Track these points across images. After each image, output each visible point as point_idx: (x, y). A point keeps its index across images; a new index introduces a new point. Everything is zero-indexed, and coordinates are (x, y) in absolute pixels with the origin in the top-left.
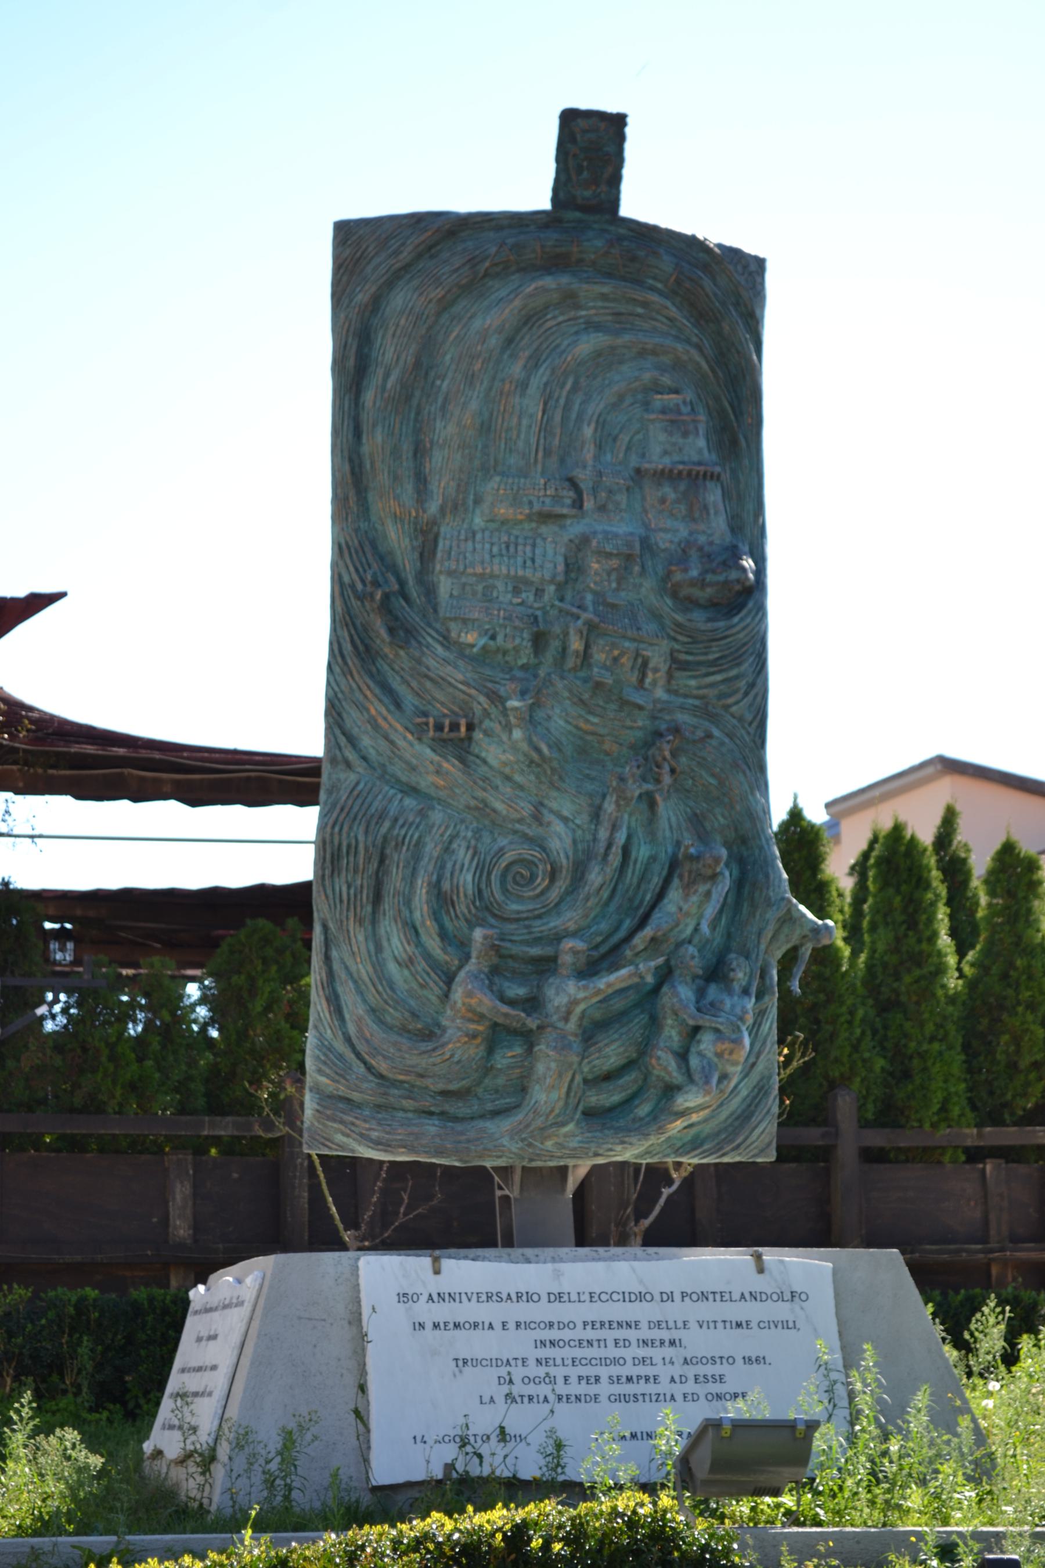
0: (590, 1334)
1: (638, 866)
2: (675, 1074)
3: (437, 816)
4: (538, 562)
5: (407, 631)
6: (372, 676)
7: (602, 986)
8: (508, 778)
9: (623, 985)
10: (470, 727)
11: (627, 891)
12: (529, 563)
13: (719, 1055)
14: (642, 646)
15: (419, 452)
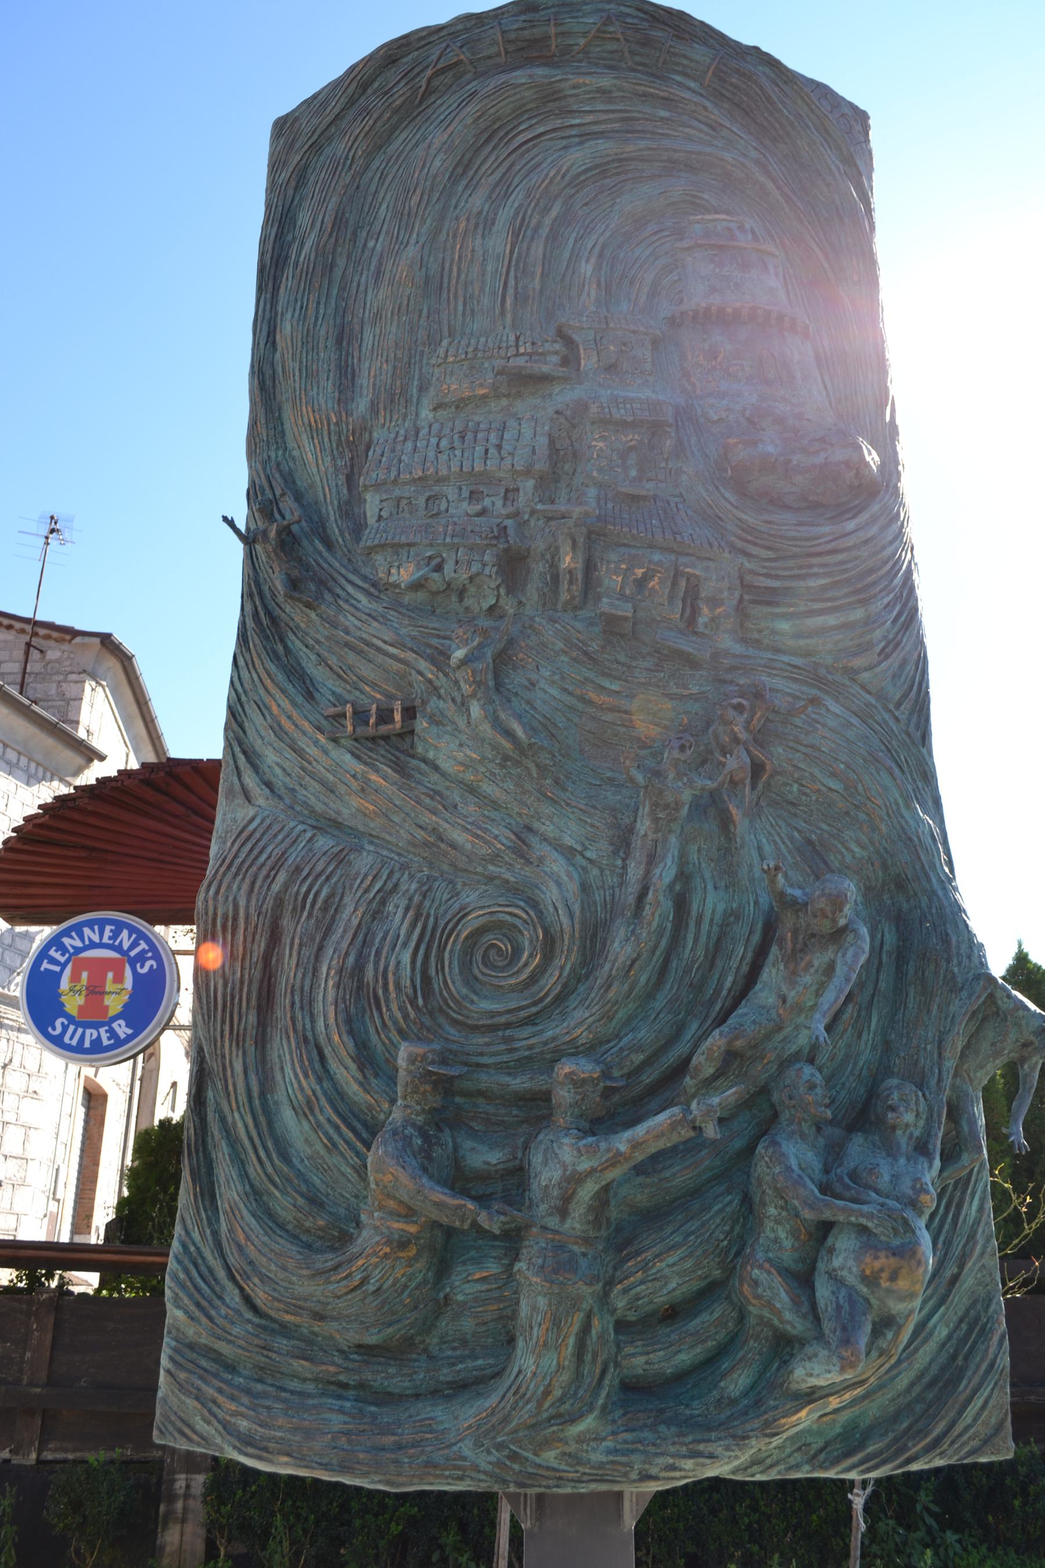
1: (705, 927)
2: (788, 1316)
3: (363, 862)
4: (507, 447)
5: (321, 583)
6: (275, 657)
7: (623, 1148)
8: (472, 790)
9: (662, 1144)
10: (410, 713)
11: (687, 971)
12: (492, 451)
13: (871, 1280)
14: (683, 560)
15: (344, 337)
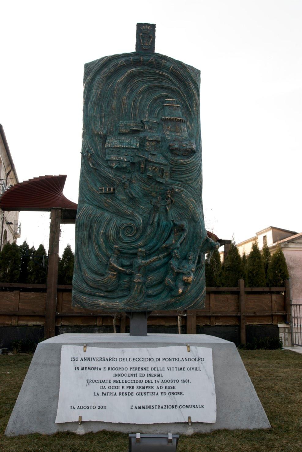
0: (132, 372)
